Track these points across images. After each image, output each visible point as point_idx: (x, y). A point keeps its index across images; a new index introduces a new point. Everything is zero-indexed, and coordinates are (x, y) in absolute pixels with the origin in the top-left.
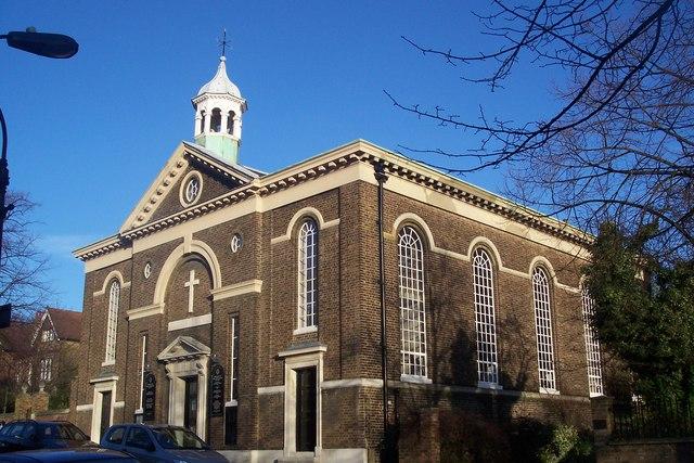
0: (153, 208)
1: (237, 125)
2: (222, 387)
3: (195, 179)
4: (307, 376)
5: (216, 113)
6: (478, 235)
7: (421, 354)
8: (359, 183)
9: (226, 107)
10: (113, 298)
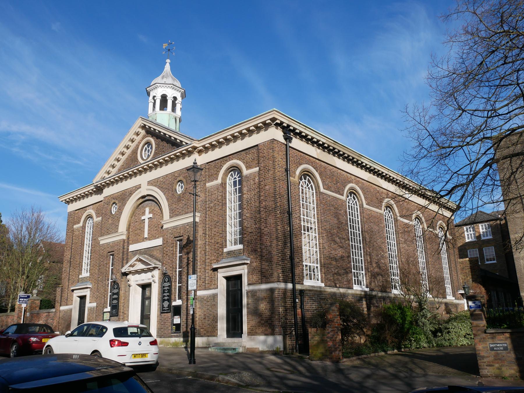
0: (119, 165)
1: (178, 107)
2: (170, 291)
3: (148, 143)
4: (234, 282)
5: (164, 98)
6: (350, 182)
7: (315, 265)
8: (273, 140)
9: (170, 93)
10: (88, 230)
